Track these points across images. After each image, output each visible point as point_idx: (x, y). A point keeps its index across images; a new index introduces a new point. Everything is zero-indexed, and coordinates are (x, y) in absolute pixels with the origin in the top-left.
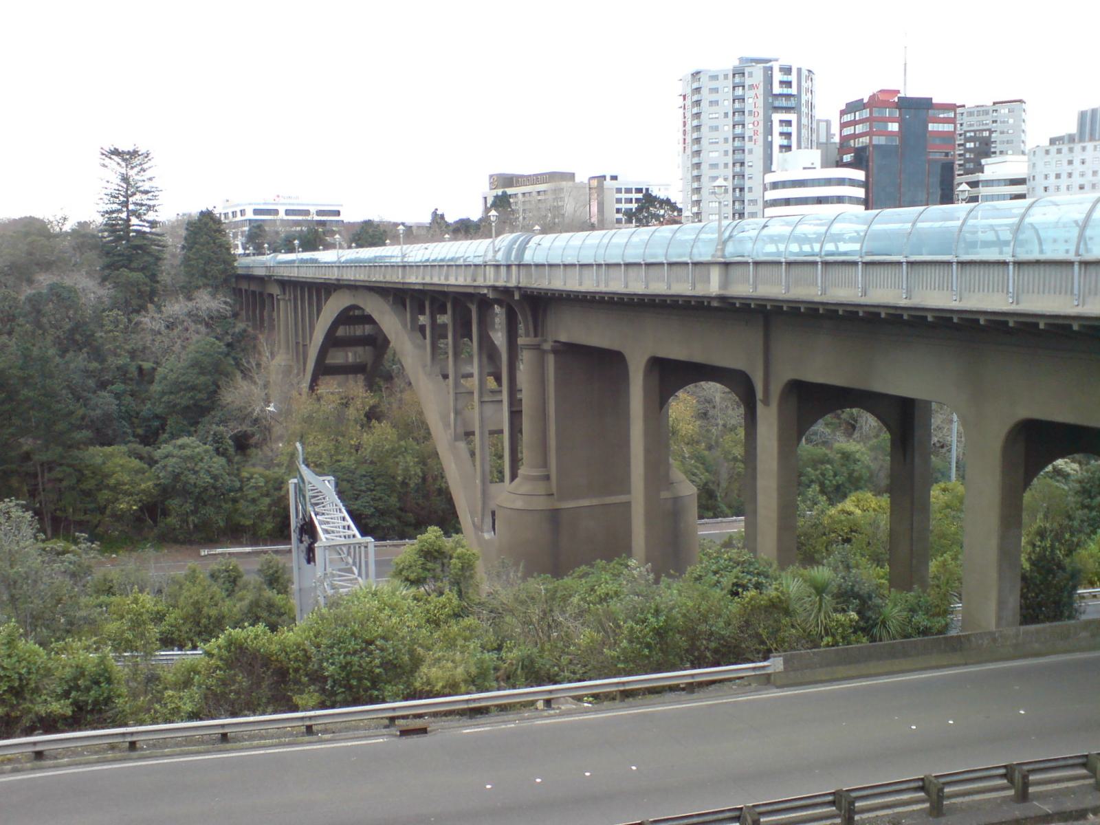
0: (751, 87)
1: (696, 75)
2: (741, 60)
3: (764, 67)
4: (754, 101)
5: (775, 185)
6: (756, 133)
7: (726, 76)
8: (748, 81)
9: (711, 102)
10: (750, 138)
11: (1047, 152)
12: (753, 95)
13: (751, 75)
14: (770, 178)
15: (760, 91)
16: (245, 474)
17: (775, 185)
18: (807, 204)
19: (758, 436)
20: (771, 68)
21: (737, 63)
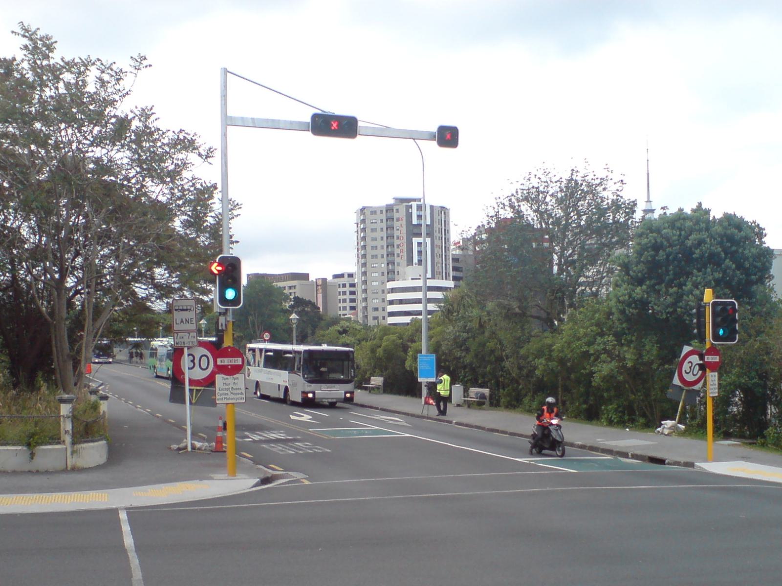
0: (398, 220)
1: (363, 210)
2: (396, 199)
3: (406, 206)
4: (400, 229)
5: (393, 290)
6: (402, 251)
7: (381, 212)
8: (396, 215)
9: (372, 229)
10: (398, 255)
11: (611, 179)
12: (400, 225)
13: (397, 211)
14: (390, 285)
15: (404, 222)
16: (503, 365)
17: (393, 290)
18: (405, 312)
19: (117, 489)
20: (411, 207)
21: (392, 202)
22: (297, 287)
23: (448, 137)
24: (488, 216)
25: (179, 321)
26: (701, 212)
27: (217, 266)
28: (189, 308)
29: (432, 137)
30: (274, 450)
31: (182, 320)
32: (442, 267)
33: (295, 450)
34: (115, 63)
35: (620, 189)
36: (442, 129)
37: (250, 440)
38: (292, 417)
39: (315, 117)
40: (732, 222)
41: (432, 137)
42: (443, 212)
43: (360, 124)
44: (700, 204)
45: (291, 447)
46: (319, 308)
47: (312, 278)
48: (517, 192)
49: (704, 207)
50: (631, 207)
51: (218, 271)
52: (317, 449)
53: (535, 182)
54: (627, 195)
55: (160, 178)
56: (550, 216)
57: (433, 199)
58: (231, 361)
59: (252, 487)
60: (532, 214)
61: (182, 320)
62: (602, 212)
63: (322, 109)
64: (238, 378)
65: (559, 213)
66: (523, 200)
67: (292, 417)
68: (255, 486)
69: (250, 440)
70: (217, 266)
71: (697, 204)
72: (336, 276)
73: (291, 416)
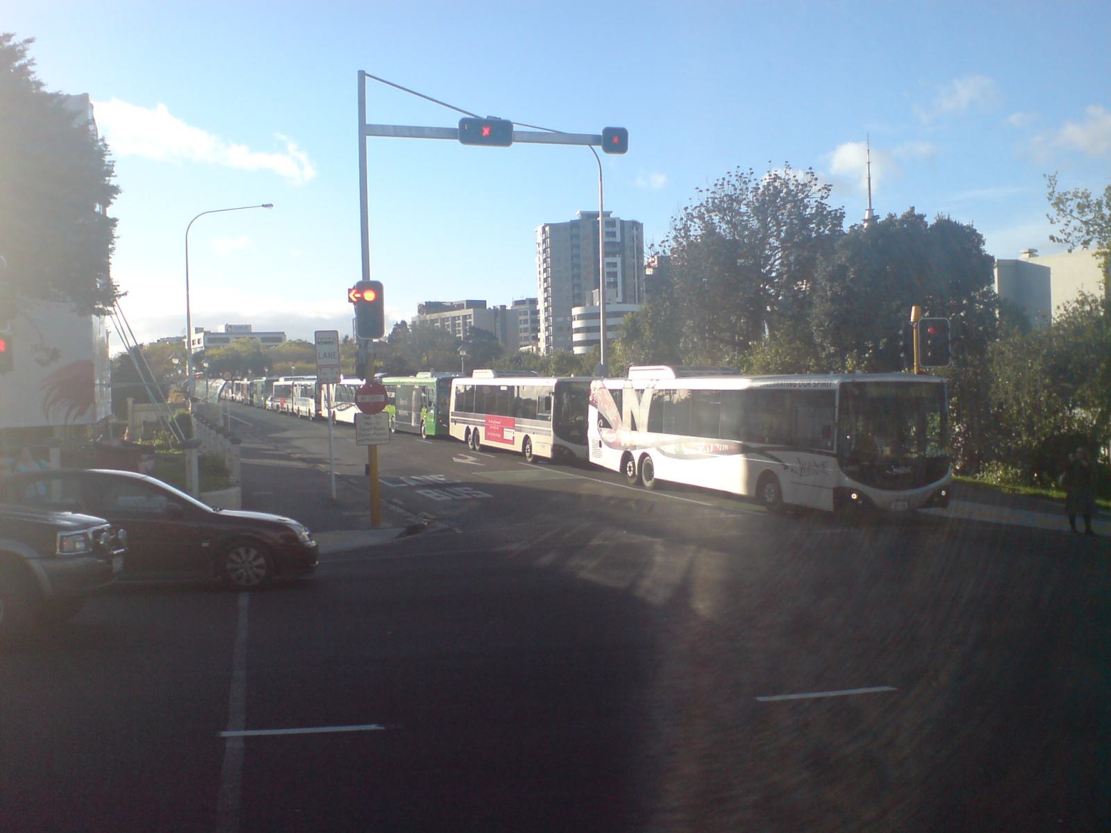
22: (472, 316)
23: (615, 140)
24: (675, 229)
25: (322, 355)
26: (913, 220)
27: (356, 293)
28: (331, 340)
29: (593, 140)
30: (429, 495)
31: (325, 353)
32: (635, 291)
33: (451, 495)
34: (1048, 216)
35: (825, 195)
36: (608, 131)
37: (405, 485)
38: (455, 460)
39: (463, 122)
40: (945, 226)
41: (593, 140)
42: (635, 228)
43: (516, 128)
44: (913, 209)
45: (448, 492)
46: (497, 339)
47: (489, 305)
48: (707, 201)
49: (917, 212)
50: (839, 217)
51: (356, 298)
52: (478, 494)
53: (729, 190)
54: (833, 204)
55: (820, 296)
56: (745, 228)
57: (623, 213)
58: (372, 398)
59: (397, 537)
60: (724, 226)
61: (325, 353)
62: (805, 221)
63: (475, 114)
64: (380, 417)
65: (754, 223)
66: (714, 211)
67: (455, 460)
68: (401, 535)
69: (405, 485)
70: (356, 293)
71: (909, 209)
72: (517, 303)
73: (454, 458)
